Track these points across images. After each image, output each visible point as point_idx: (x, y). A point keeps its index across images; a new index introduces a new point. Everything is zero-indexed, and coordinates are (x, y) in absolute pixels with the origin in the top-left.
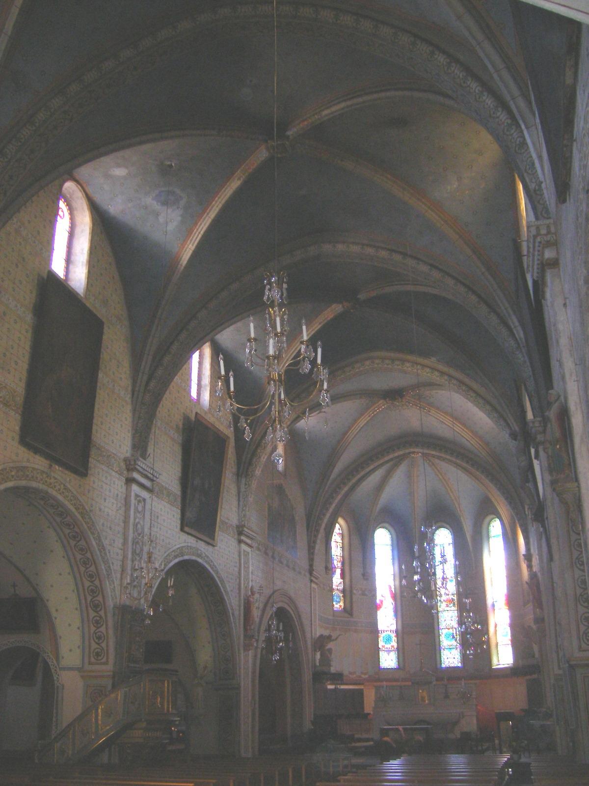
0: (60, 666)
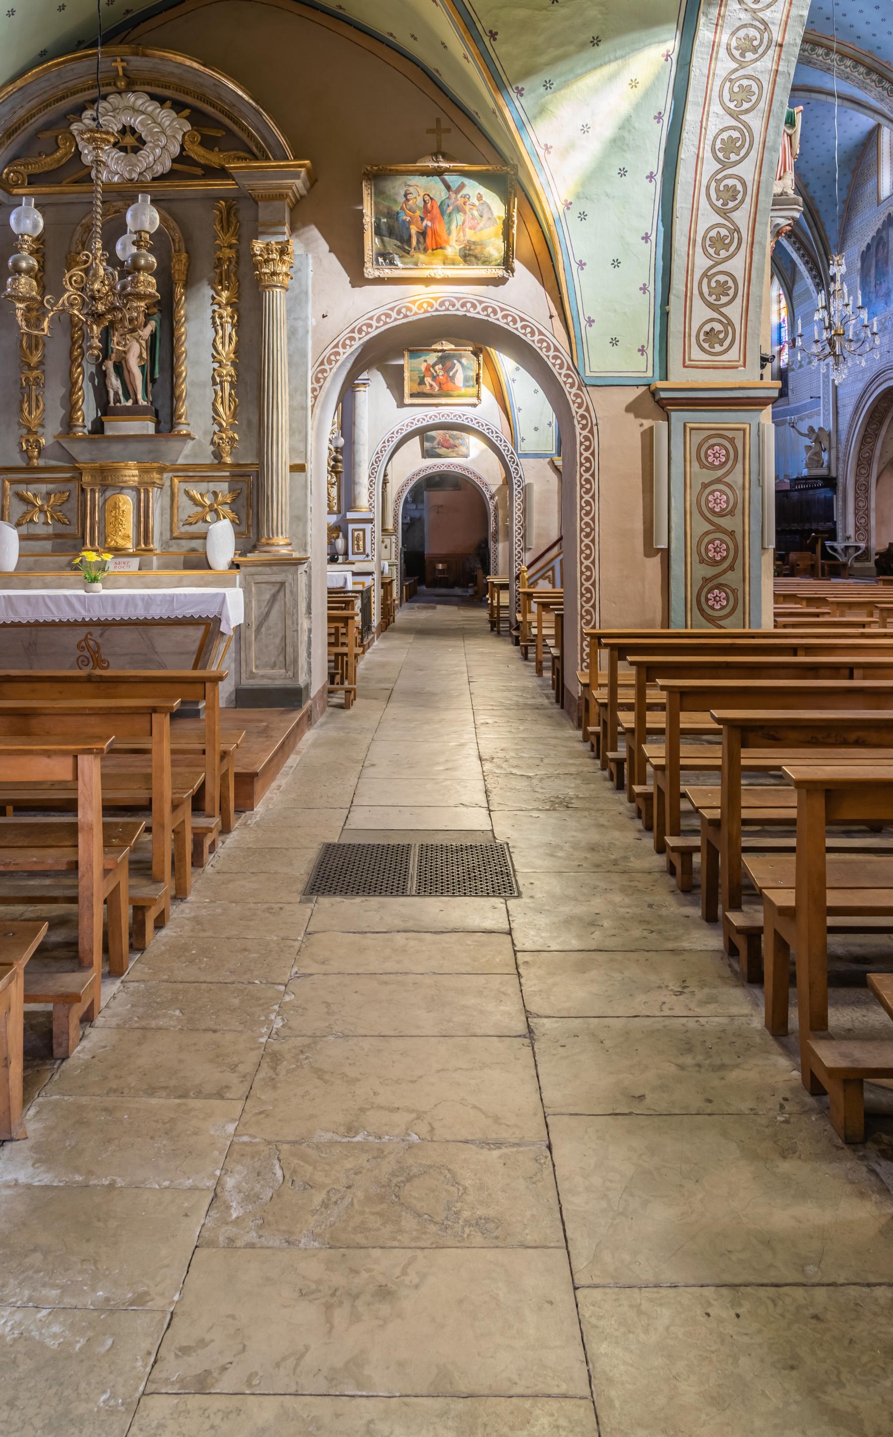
0: (519, 452)
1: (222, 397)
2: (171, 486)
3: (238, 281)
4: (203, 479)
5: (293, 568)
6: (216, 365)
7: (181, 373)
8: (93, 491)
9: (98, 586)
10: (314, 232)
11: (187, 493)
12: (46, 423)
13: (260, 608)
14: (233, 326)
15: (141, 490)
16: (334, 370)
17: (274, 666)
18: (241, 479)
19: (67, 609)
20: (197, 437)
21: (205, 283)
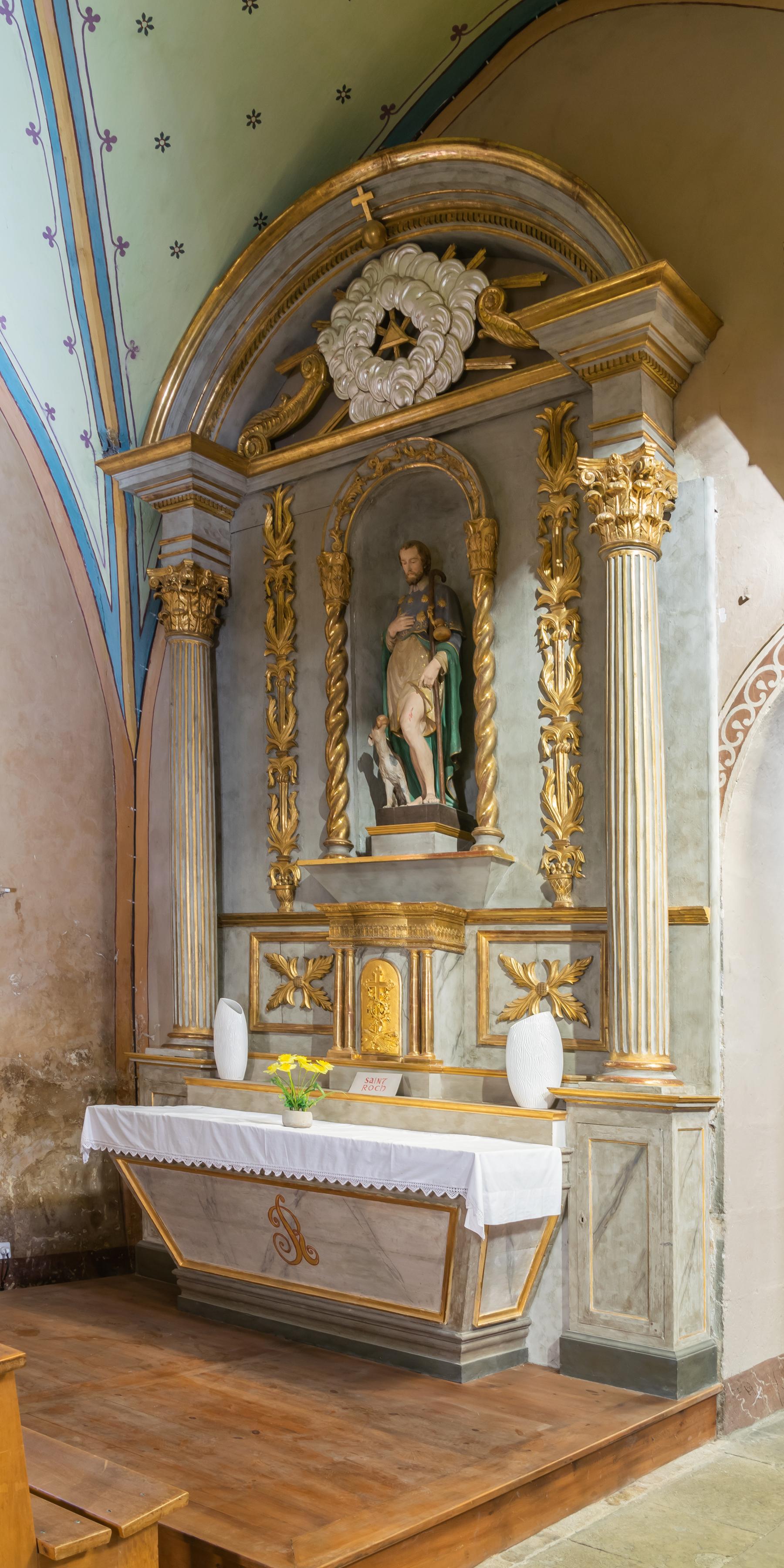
1: (555, 782)
2: (477, 950)
3: (579, 554)
4: (527, 937)
5: (662, 1118)
6: (546, 721)
7: (486, 738)
8: (344, 953)
9: (305, 1116)
10: (718, 433)
11: (501, 961)
12: (302, 842)
13: (602, 1189)
14: (573, 642)
15: (416, 951)
16: (765, 711)
17: (627, 1307)
18: (592, 937)
19: (241, 1149)
20: (516, 859)
21: (526, 568)
